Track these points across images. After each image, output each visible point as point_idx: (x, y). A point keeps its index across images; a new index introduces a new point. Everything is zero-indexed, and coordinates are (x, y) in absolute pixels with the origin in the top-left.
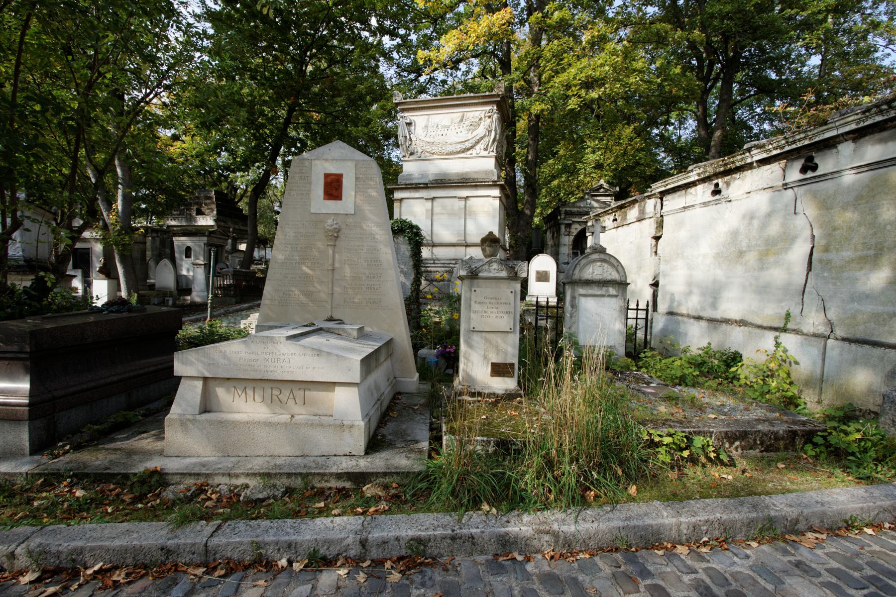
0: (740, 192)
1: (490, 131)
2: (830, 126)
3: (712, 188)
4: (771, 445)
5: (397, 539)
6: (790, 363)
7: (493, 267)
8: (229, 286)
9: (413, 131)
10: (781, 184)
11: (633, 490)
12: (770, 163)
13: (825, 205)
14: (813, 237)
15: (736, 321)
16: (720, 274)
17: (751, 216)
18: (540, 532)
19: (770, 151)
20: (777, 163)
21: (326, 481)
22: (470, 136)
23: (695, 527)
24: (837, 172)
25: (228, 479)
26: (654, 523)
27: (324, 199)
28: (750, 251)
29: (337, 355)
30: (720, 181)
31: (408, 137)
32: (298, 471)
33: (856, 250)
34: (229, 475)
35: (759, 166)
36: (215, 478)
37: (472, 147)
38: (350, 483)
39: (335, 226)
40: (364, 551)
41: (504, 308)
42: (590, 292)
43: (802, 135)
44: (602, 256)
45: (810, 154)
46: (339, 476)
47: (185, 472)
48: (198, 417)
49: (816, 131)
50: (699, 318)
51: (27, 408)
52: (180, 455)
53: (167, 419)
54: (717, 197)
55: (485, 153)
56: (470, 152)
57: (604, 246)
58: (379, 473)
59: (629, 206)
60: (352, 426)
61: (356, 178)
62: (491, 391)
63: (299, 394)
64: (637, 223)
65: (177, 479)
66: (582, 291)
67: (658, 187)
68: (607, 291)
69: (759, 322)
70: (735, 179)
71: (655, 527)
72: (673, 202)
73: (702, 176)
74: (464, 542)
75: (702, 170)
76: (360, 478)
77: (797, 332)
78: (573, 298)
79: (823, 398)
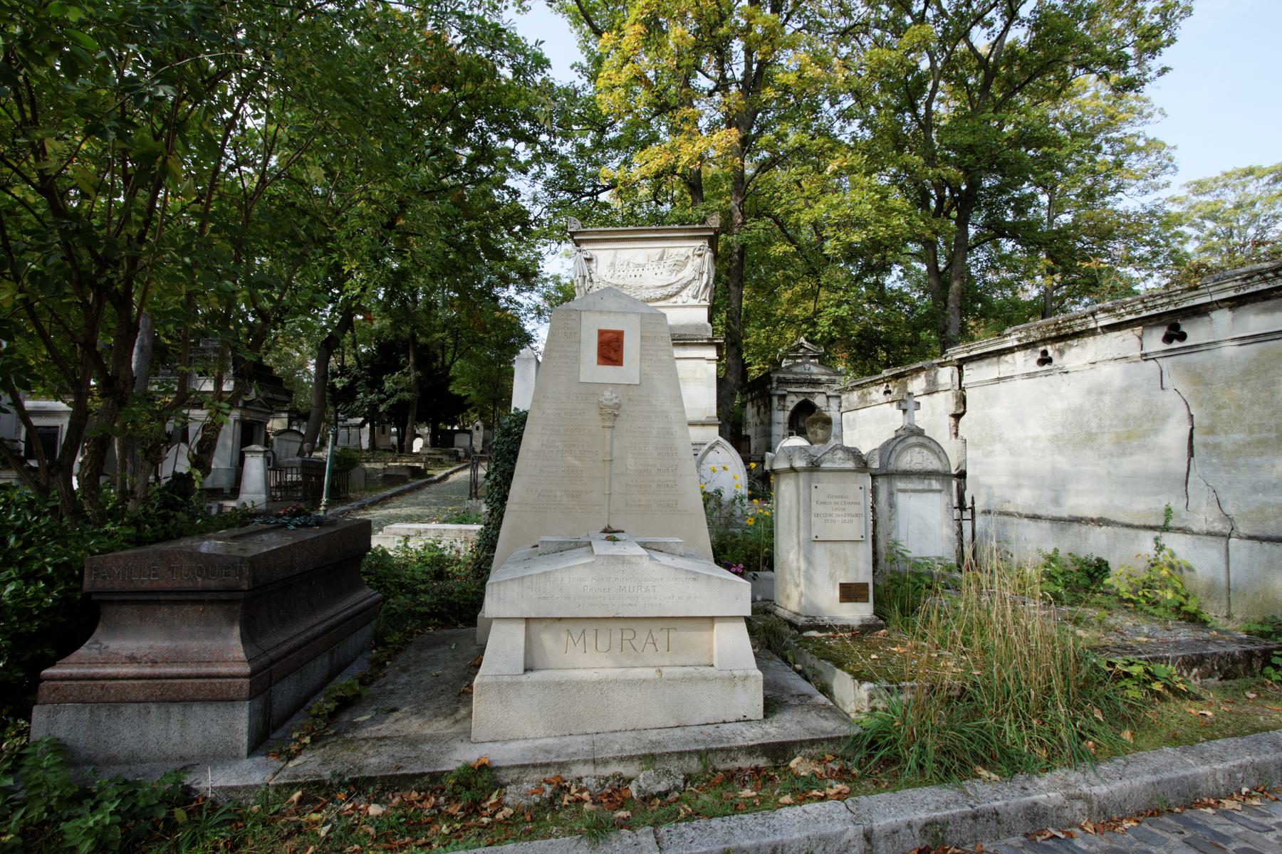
0: (1081, 362)
1: (702, 274)
2: (1202, 291)
3: (1039, 356)
4: (1229, 671)
5: (909, 825)
6: (1181, 570)
8: (294, 485)
9: (594, 270)
10: (1138, 353)
11: (1127, 735)
12: (1119, 330)
13: (1198, 378)
14: (1191, 416)
15: (1092, 520)
16: (1062, 462)
17: (1097, 391)
18: (1071, 798)
19: (1122, 316)
20: (1130, 330)
21: (733, 759)
22: (673, 279)
23: (1230, 774)
24: (1214, 343)
25: (592, 768)
26: (1188, 773)
27: (599, 364)
28: (1103, 433)
29: (720, 578)
30: (1049, 348)
31: (588, 277)
32: (694, 747)
33: (1251, 432)
34: (594, 762)
35: (1104, 333)
36: (572, 768)
37: (677, 293)
38: (765, 759)
39: (615, 401)
40: (869, 848)
41: (853, 509)
42: (910, 486)
43: (1165, 300)
44: (921, 440)
45: (1173, 321)
46: (750, 750)
47: (526, 762)
48: (524, 678)
49: (1183, 296)
50: (1035, 517)
51: (247, 681)
52: (496, 738)
53: (478, 685)
54: (1046, 367)
55: (695, 302)
56: (674, 299)
57: (921, 426)
58: (804, 741)
59: (911, 375)
60: (746, 678)
61: (642, 337)
62: (845, 623)
63: (661, 637)
64: (926, 397)
65: (514, 774)
66: (901, 484)
67: (957, 352)
68: (930, 484)
69: (1128, 520)
70: (1071, 346)
71: (1190, 779)
72: (973, 374)
73: (1025, 341)
74: (988, 821)
75: (1024, 334)
76: (779, 752)
77: (1183, 531)
78: (891, 494)
79: (1233, 611)
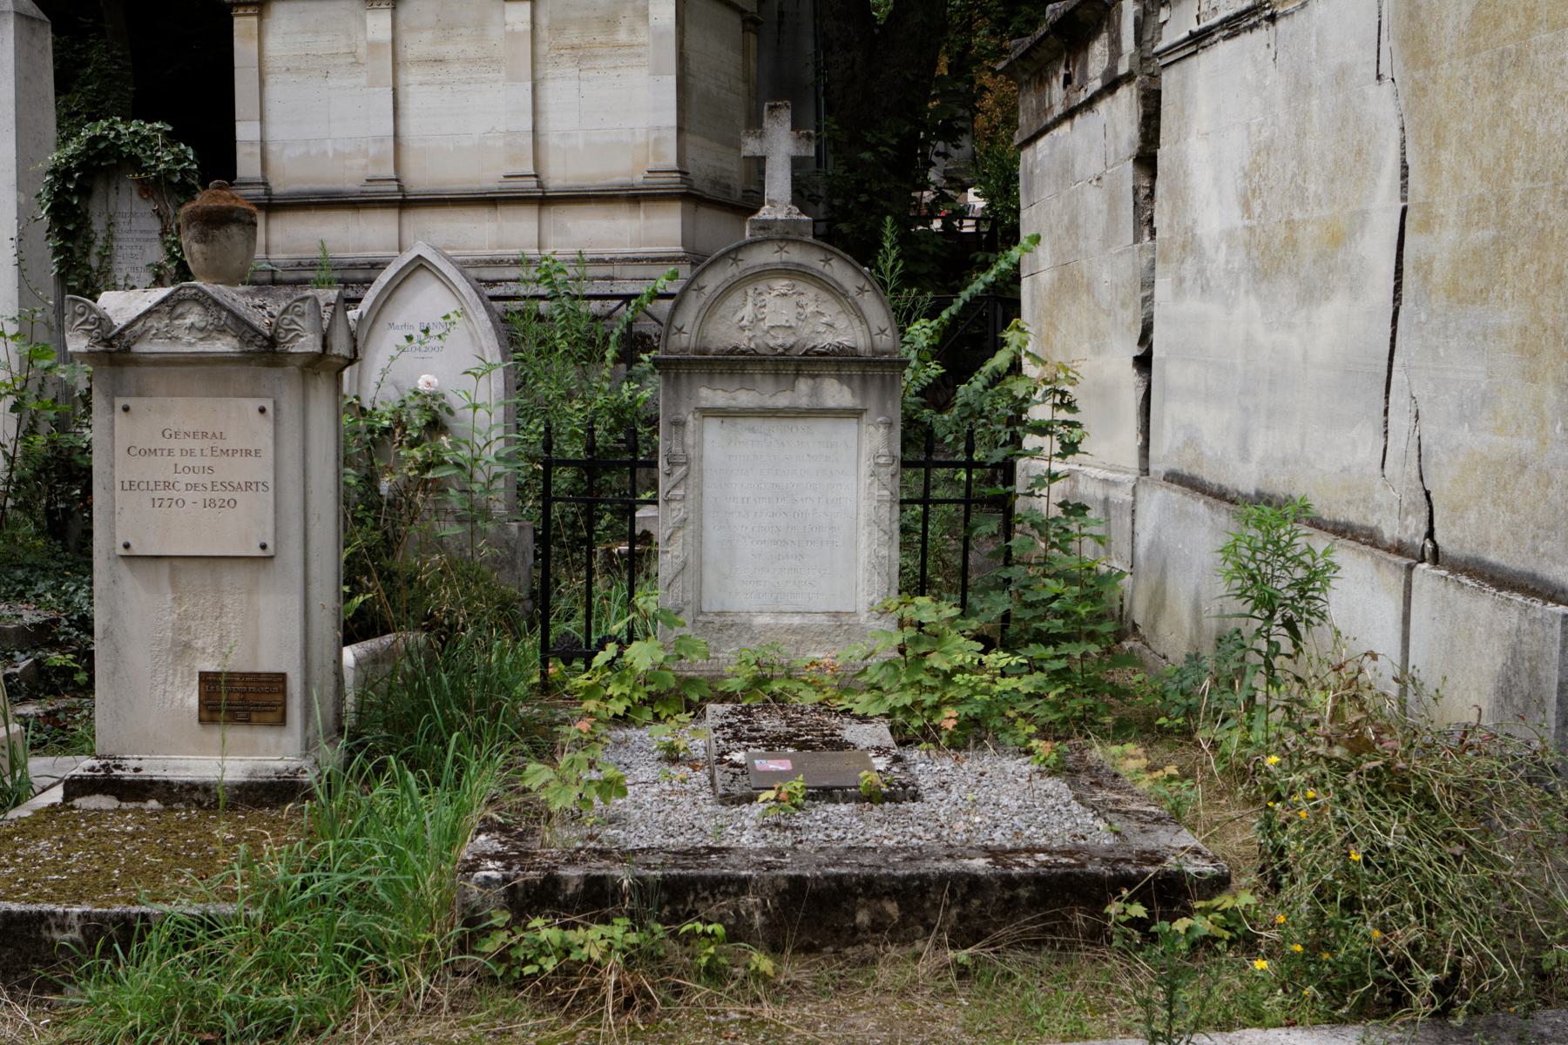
7: (188, 321)
42: (744, 398)
66: (712, 395)
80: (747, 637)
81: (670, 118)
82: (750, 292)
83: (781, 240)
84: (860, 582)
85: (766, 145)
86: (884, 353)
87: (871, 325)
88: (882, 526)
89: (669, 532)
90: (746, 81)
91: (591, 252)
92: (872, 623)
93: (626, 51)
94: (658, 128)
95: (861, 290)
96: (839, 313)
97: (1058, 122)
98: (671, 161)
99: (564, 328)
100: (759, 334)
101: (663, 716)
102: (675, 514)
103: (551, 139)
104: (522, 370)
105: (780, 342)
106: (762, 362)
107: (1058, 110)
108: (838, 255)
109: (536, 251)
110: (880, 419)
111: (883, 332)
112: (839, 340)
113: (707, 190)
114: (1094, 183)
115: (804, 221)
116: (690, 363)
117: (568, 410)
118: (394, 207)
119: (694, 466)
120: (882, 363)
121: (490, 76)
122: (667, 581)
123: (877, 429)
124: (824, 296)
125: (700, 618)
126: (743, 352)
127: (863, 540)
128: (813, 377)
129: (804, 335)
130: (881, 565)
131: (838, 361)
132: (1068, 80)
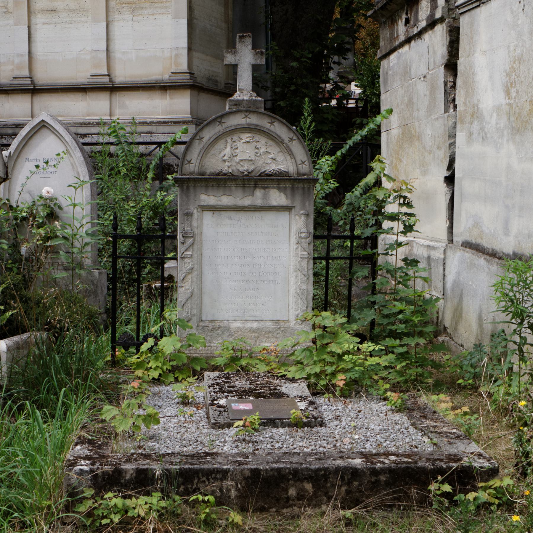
80: (227, 334)
81: (184, 43)
82: (229, 141)
83: (246, 111)
84: (291, 304)
85: (237, 58)
86: (304, 175)
87: (297, 159)
88: (303, 272)
89: (183, 275)
90: (226, 22)
91: (139, 118)
92: (298, 326)
93: (159, 5)
94: (177, 49)
95: (291, 139)
96: (279, 152)
97: (401, 45)
98: (184, 66)
99: (124, 161)
100: (234, 164)
101: (180, 379)
102: (186, 265)
103: (117, 55)
104: (101, 184)
105: (245, 168)
106: (235, 180)
107: (402, 38)
108: (278, 120)
109: (109, 117)
110: (302, 212)
111: (303, 163)
112: (279, 167)
113: (204, 83)
114: (422, 79)
115: (259, 101)
116: (195, 180)
117: (127, 207)
118: (28, 93)
119: (197, 238)
120: (303, 180)
121: (82, 19)
122: (182, 303)
123: (300, 217)
124: (270, 143)
125: (201, 324)
126: (225, 174)
127: (293, 280)
128: (264, 188)
129: (259, 165)
130: (302, 294)
131: (278, 179)
132: (407, 21)
